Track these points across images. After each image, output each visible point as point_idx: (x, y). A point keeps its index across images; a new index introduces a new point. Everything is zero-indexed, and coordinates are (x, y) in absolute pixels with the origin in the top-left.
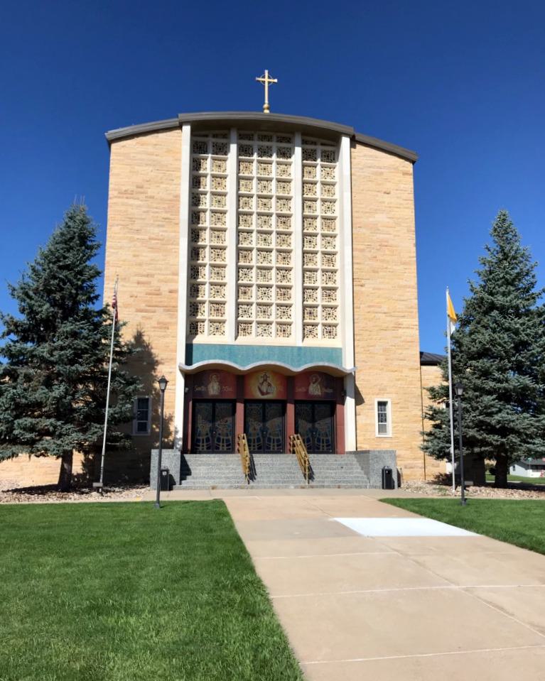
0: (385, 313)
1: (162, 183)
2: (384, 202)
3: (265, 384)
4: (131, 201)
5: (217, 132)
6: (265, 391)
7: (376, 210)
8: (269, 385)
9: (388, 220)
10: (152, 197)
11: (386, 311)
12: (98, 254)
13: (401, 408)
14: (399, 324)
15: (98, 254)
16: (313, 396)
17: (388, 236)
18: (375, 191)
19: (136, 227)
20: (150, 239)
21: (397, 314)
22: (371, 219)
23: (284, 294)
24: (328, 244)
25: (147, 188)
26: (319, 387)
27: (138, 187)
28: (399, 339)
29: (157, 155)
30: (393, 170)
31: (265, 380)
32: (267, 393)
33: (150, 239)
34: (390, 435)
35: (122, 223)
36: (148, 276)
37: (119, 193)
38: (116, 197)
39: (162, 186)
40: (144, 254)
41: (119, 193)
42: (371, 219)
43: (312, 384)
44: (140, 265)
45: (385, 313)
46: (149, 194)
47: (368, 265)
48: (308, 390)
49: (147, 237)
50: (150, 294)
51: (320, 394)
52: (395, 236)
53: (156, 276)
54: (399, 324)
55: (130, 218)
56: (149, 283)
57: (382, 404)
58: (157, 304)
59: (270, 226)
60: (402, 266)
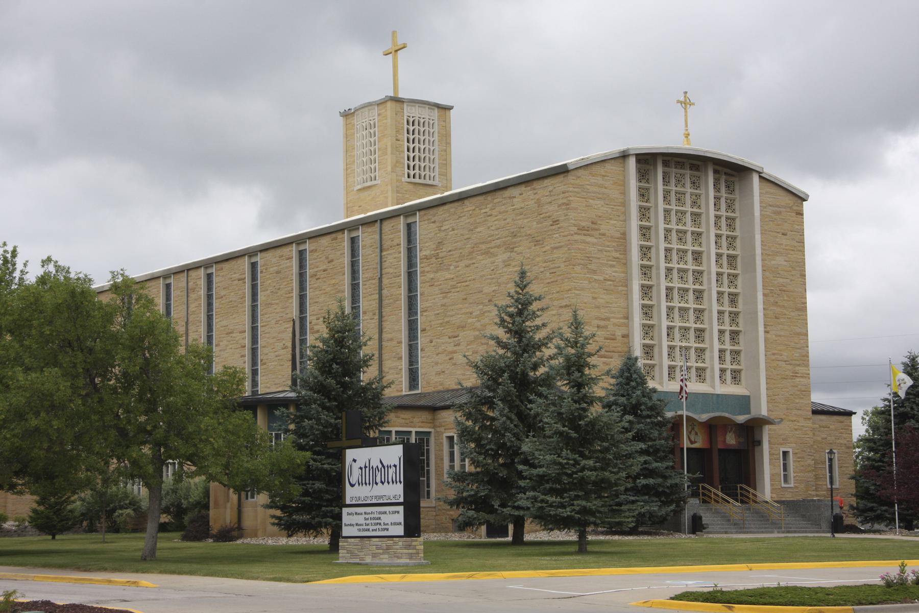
0: (785, 361)
1: (611, 219)
2: (782, 244)
3: (693, 432)
4: (589, 239)
5: (420, 105)
6: (693, 440)
7: (777, 252)
8: (696, 434)
9: (785, 263)
10: (604, 235)
11: (785, 358)
12: (15, 247)
13: (799, 458)
14: (796, 373)
15: (15, 247)
16: (731, 445)
17: (785, 280)
18: (775, 232)
19: (593, 267)
20: (605, 280)
21: (794, 362)
22: (773, 262)
23: (699, 337)
24: (730, 284)
25: (600, 224)
26: (733, 436)
27: (593, 223)
28: (796, 389)
29: (606, 188)
30: (789, 210)
31: (693, 429)
32: (695, 442)
33: (605, 280)
34: (792, 485)
35: (582, 262)
36: (604, 320)
37: (578, 229)
38: (576, 233)
39: (612, 222)
40: (601, 296)
41: (578, 229)
42: (773, 262)
43: (728, 433)
44: (598, 307)
45: (785, 361)
46: (602, 231)
47: (771, 310)
48: (725, 439)
49: (601, 278)
50: (607, 339)
51: (735, 443)
52: (791, 280)
53: (612, 320)
54: (796, 373)
55: (588, 257)
56: (605, 327)
57: (785, 454)
58: (614, 349)
59: (686, 263)
60: (797, 313)
